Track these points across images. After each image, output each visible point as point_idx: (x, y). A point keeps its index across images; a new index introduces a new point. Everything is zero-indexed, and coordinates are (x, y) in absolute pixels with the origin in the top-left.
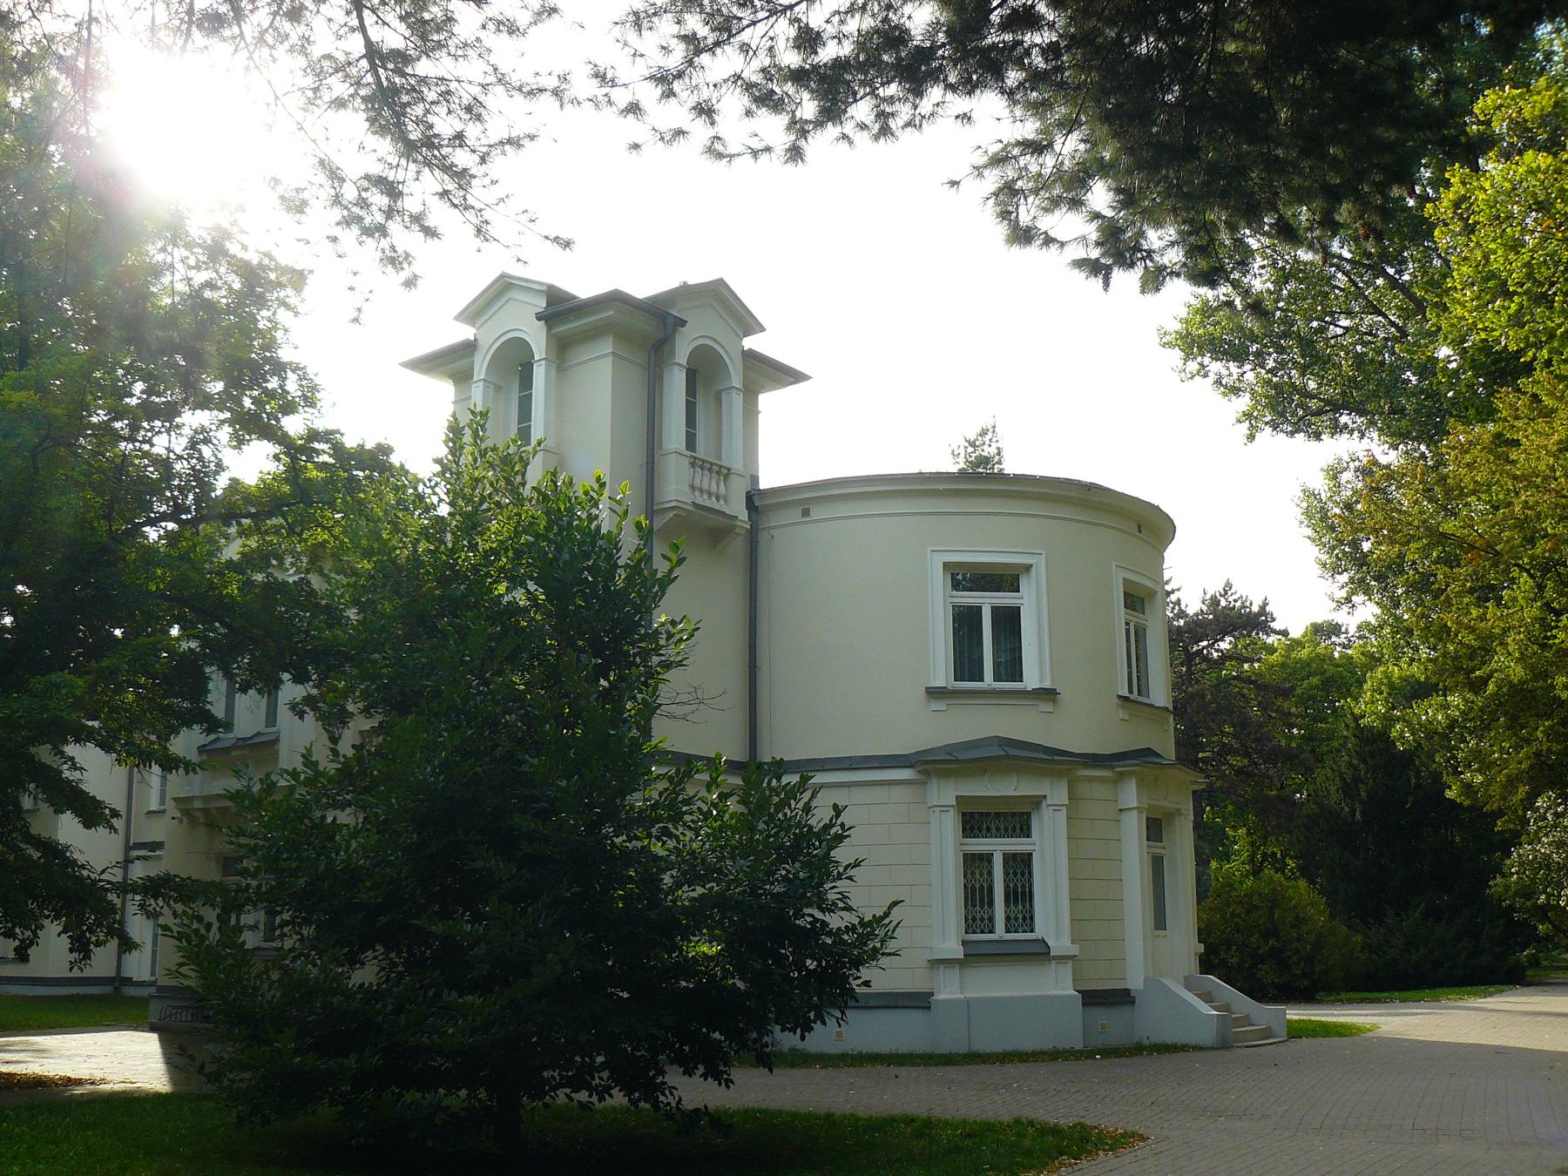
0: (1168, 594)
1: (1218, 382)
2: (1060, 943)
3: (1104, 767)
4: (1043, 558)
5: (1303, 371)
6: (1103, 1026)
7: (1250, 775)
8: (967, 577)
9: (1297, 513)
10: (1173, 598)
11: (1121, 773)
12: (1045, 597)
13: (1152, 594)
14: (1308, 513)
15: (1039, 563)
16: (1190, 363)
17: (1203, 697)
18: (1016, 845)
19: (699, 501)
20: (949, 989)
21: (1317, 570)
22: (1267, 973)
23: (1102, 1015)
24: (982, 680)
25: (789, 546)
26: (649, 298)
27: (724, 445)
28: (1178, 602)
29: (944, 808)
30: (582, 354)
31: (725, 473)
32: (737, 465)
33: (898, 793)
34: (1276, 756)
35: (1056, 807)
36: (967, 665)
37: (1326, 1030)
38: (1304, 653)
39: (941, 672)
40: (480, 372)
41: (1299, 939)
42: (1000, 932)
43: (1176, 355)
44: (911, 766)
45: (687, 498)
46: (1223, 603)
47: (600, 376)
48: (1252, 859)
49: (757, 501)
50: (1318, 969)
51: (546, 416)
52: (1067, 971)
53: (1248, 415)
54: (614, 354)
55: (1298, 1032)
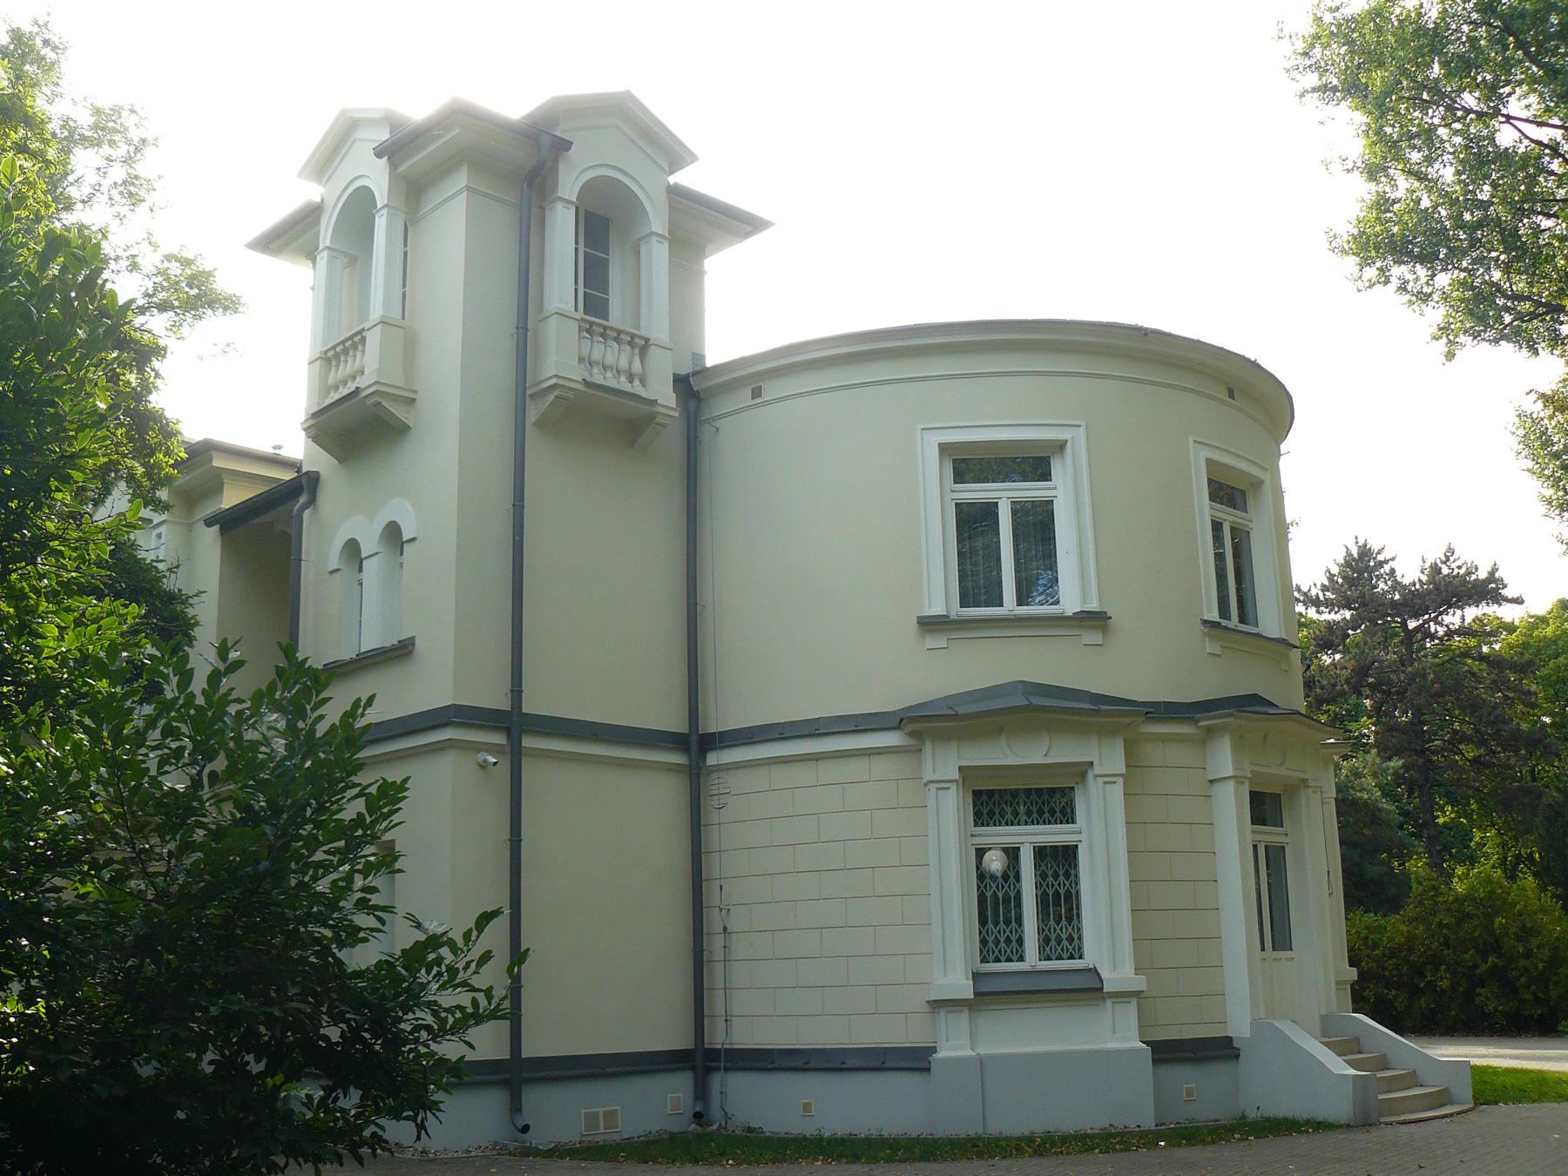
0: (1381, 564)
1: (1403, 288)
2: (1118, 972)
3: (1183, 720)
4: (1082, 431)
5: (1507, 269)
6: (1189, 1092)
7: (1488, 765)
8: (968, 464)
9: (1513, 443)
10: (1387, 568)
11: (1209, 729)
12: (1086, 485)
13: (1257, 484)
14: (1526, 441)
15: (1077, 439)
16: (1367, 269)
17: (1424, 676)
18: (1053, 834)
19: (598, 378)
20: (955, 1044)
21: (1542, 508)
22: (1489, 999)
23: (1186, 1077)
24: (1001, 605)
25: (743, 441)
26: (528, 117)
27: (643, 310)
28: (1393, 571)
29: (942, 785)
30: (434, 197)
31: (643, 346)
32: (657, 327)
33: (880, 766)
34: (1514, 741)
35: (1109, 779)
36: (977, 583)
37: (1536, 1089)
38: (1549, 631)
39: (940, 597)
40: (325, 239)
41: (1528, 954)
42: (1032, 957)
43: (1352, 262)
44: (898, 728)
45: (575, 373)
46: (1445, 571)
47: (453, 220)
48: (1503, 862)
49: (696, 390)
50: (1554, 993)
51: (387, 279)
52: (1129, 1015)
53: (1444, 329)
54: (468, 188)
55: (1492, 1090)
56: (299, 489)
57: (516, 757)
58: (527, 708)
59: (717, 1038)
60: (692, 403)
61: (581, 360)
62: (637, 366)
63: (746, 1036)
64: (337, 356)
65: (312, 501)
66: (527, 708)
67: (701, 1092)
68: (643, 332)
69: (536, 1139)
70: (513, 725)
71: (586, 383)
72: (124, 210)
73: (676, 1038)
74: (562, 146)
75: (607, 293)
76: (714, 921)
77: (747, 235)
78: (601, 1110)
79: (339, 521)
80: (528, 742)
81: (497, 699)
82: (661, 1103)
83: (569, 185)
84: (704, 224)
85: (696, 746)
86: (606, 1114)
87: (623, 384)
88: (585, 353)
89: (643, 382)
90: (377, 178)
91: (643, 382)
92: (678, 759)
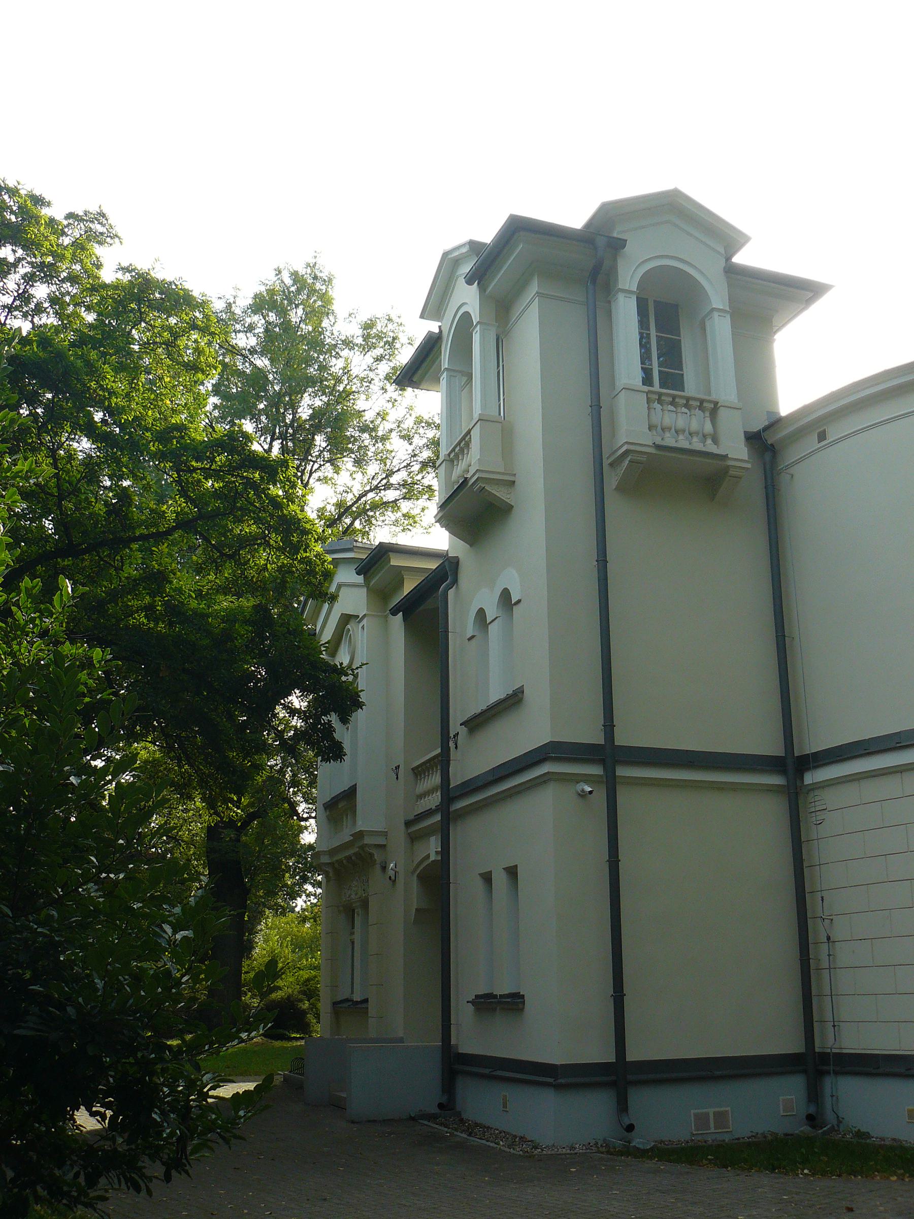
19: (669, 441)
25: (819, 487)
31: (714, 410)
32: (725, 389)
49: (770, 443)
56: (446, 571)
57: (611, 785)
58: (621, 739)
59: (826, 1042)
60: (768, 456)
61: (650, 428)
62: (708, 427)
63: (854, 1040)
64: (457, 456)
65: (455, 581)
66: (621, 739)
67: (814, 1095)
68: (714, 397)
69: (638, 1142)
70: (608, 758)
71: (658, 447)
72: (395, 395)
73: (785, 1041)
74: (617, 245)
75: (682, 370)
76: (818, 931)
77: (809, 302)
78: (711, 1111)
79: (471, 598)
80: (622, 771)
81: (593, 735)
82: (773, 1107)
83: (629, 276)
84: (770, 298)
85: (792, 768)
86: (718, 1115)
87: (696, 445)
88: (656, 419)
89: (715, 441)
90: (467, 298)
91: (715, 441)
92: (776, 780)
